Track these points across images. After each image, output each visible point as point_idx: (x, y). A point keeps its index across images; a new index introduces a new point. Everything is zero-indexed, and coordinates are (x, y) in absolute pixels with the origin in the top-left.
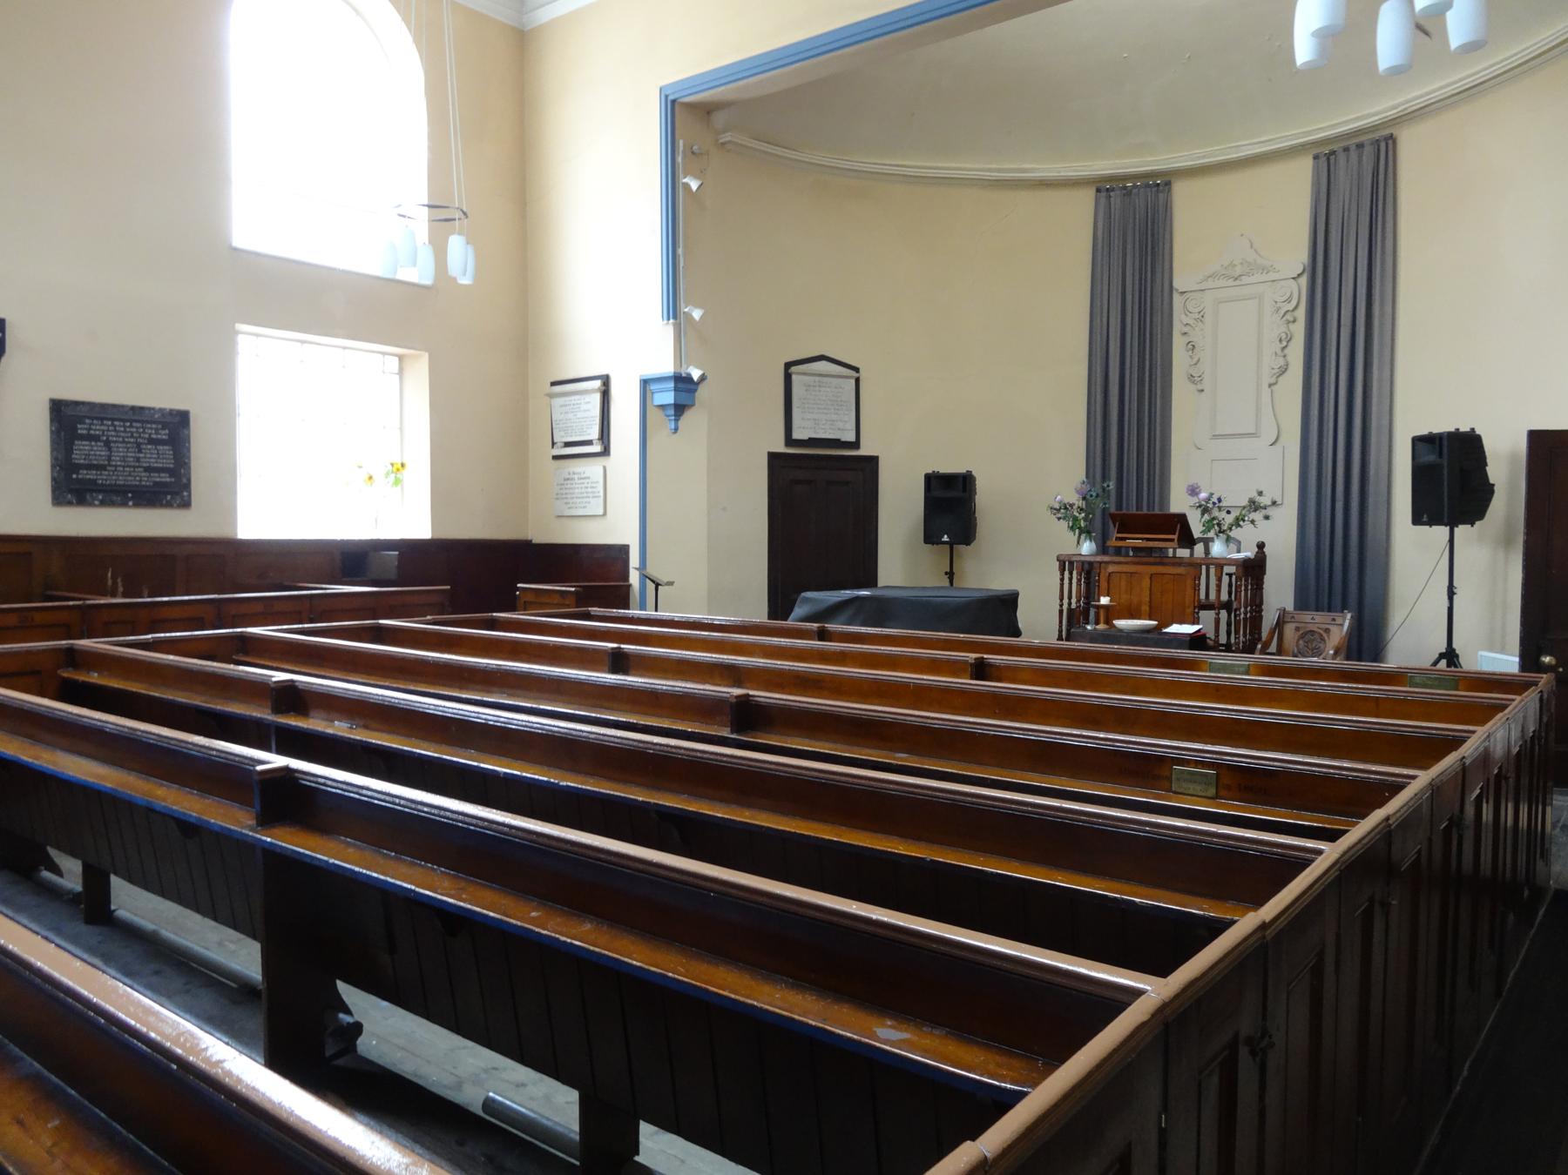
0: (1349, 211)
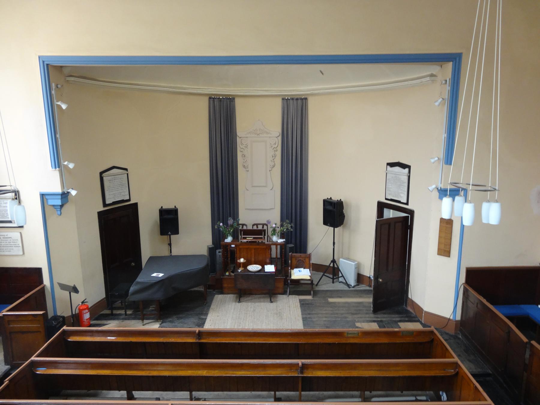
0: (294, 119)
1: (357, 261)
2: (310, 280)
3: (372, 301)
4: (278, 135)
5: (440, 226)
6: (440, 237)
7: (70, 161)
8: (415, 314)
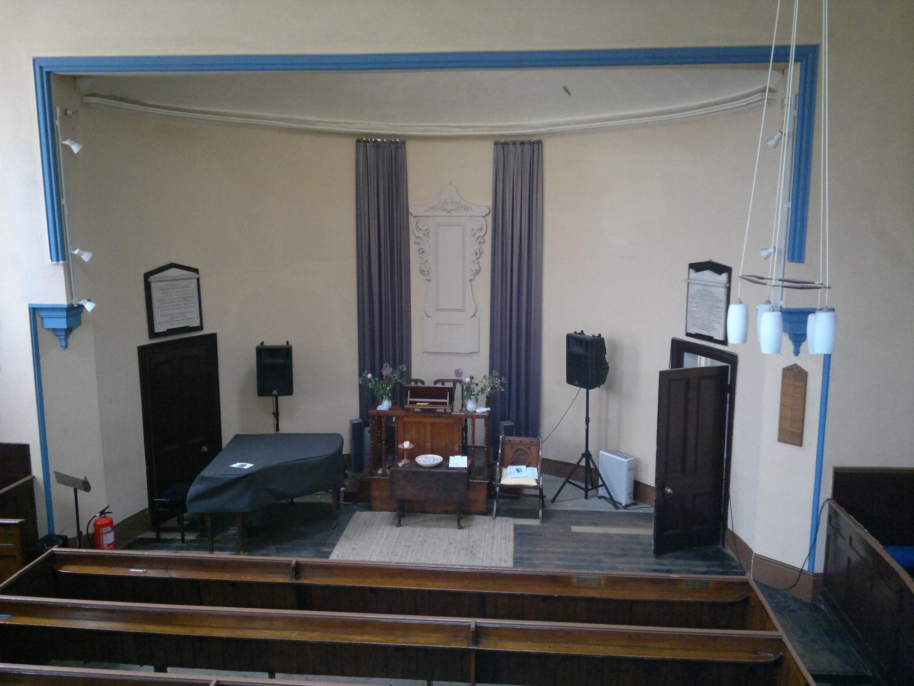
1: (632, 457)
2: (536, 489)
3: (652, 534)
4: (488, 213)
5: (783, 384)
6: (782, 406)
7: (84, 249)
8: (738, 561)
